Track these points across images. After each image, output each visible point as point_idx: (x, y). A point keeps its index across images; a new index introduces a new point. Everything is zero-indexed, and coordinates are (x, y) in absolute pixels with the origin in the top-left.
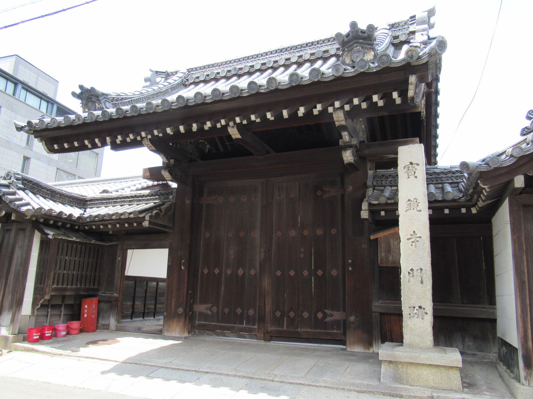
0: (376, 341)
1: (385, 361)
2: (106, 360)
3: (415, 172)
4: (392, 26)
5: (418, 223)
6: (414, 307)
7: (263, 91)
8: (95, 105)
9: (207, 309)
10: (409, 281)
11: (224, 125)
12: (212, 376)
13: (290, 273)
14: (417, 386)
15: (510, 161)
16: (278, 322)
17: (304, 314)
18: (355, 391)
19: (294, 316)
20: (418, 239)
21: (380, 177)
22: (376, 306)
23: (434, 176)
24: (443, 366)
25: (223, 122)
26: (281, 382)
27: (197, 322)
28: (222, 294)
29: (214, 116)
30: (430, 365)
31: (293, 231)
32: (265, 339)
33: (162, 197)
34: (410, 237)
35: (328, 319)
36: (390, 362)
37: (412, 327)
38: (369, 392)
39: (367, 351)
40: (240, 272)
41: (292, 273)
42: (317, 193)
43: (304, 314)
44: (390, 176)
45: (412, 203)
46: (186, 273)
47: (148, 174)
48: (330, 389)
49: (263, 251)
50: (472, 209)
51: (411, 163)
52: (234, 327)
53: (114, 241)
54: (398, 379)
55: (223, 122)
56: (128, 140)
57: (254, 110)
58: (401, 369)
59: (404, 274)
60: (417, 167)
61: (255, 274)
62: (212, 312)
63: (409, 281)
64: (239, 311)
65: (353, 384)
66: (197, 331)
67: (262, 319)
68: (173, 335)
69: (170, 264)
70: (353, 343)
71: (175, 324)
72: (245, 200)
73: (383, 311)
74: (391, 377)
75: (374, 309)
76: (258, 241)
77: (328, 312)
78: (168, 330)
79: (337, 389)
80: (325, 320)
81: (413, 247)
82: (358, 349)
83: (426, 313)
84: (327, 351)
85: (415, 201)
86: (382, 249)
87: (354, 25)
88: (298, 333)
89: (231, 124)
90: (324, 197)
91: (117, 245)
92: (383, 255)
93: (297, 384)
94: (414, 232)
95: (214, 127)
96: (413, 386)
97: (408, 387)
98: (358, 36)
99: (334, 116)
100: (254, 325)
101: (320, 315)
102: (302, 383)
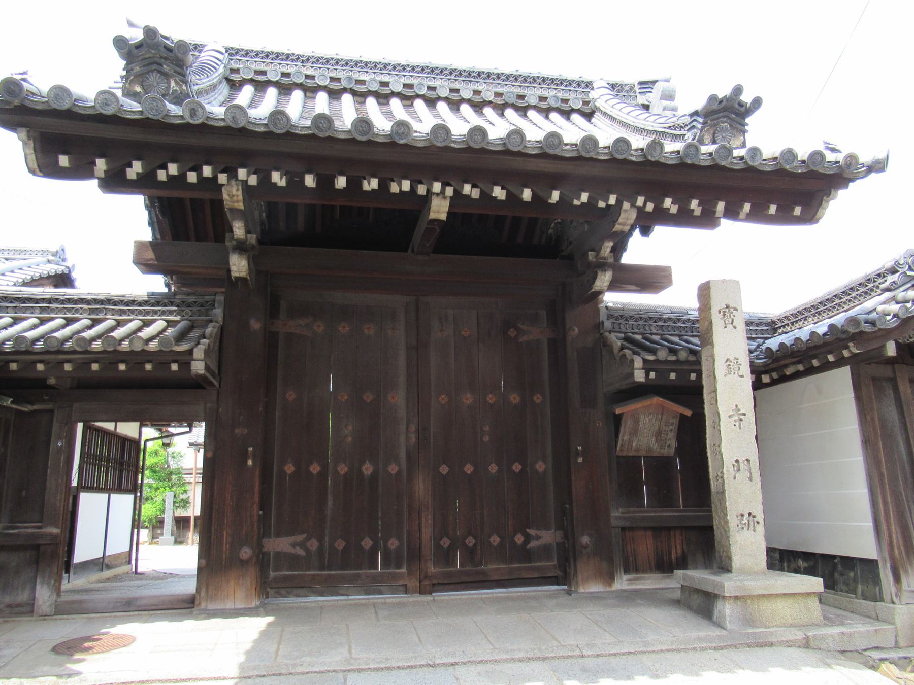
2: (190, 679)
4: (232, 52)
6: (742, 515)
7: (633, 159)
8: (169, 83)
9: (294, 545)
10: (735, 478)
11: (174, 176)
12: (480, 668)
13: (465, 469)
16: (445, 557)
17: (492, 540)
18: (710, 648)
19: (475, 545)
20: (742, 417)
22: (617, 518)
23: (688, 325)
24: (799, 594)
26: (598, 656)
27: (272, 574)
28: (329, 513)
29: (601, 186)
31: (469, 395)
32: (422, 592)
33: (187, 310)
35: (533, 544)
36: (737, 598)
39: (608, 589)
40: (368, 469)
41: (469, 469)
42: (509, 333)
43: (492, 540)
46: (257, 473)
47: (150, 255)
49: (413, 428)
50: (763, 376)
51: (727, 307)
52: (358, 576)
53: (43, 401)
54: (749, 621)
55: (173, 169)
56: (162, 175)
57: (311, 163)
60: (735, 313)
61: (399, 473)
62: (307, 550)
63: (735, 478)
64: (367, 543)
65: (699, 639)
66: (271, 592)
67: (415, 555)
68: (229, 605)
69: (210, 455)
70: (587, 580)
71: (232, 583)
72: (372, 332)
73: (627, 524)
75: (614, 522)
76: (402, 412)
77: (532, 532)
78: (212, 598)
79: (685, 650)
80: (528, 547)
82: (595, 587)
83: (758, 523)
86: (627, 430)
87: (738, 90)
88: (483, 573)
89: (626, 205)
90: (521, 340)
91: (52, 411)
93: (623, 654)
94: (736, 406)
95: (591, 204)
98: (733, 107)
100: (399, 567)
101: (519, 539)
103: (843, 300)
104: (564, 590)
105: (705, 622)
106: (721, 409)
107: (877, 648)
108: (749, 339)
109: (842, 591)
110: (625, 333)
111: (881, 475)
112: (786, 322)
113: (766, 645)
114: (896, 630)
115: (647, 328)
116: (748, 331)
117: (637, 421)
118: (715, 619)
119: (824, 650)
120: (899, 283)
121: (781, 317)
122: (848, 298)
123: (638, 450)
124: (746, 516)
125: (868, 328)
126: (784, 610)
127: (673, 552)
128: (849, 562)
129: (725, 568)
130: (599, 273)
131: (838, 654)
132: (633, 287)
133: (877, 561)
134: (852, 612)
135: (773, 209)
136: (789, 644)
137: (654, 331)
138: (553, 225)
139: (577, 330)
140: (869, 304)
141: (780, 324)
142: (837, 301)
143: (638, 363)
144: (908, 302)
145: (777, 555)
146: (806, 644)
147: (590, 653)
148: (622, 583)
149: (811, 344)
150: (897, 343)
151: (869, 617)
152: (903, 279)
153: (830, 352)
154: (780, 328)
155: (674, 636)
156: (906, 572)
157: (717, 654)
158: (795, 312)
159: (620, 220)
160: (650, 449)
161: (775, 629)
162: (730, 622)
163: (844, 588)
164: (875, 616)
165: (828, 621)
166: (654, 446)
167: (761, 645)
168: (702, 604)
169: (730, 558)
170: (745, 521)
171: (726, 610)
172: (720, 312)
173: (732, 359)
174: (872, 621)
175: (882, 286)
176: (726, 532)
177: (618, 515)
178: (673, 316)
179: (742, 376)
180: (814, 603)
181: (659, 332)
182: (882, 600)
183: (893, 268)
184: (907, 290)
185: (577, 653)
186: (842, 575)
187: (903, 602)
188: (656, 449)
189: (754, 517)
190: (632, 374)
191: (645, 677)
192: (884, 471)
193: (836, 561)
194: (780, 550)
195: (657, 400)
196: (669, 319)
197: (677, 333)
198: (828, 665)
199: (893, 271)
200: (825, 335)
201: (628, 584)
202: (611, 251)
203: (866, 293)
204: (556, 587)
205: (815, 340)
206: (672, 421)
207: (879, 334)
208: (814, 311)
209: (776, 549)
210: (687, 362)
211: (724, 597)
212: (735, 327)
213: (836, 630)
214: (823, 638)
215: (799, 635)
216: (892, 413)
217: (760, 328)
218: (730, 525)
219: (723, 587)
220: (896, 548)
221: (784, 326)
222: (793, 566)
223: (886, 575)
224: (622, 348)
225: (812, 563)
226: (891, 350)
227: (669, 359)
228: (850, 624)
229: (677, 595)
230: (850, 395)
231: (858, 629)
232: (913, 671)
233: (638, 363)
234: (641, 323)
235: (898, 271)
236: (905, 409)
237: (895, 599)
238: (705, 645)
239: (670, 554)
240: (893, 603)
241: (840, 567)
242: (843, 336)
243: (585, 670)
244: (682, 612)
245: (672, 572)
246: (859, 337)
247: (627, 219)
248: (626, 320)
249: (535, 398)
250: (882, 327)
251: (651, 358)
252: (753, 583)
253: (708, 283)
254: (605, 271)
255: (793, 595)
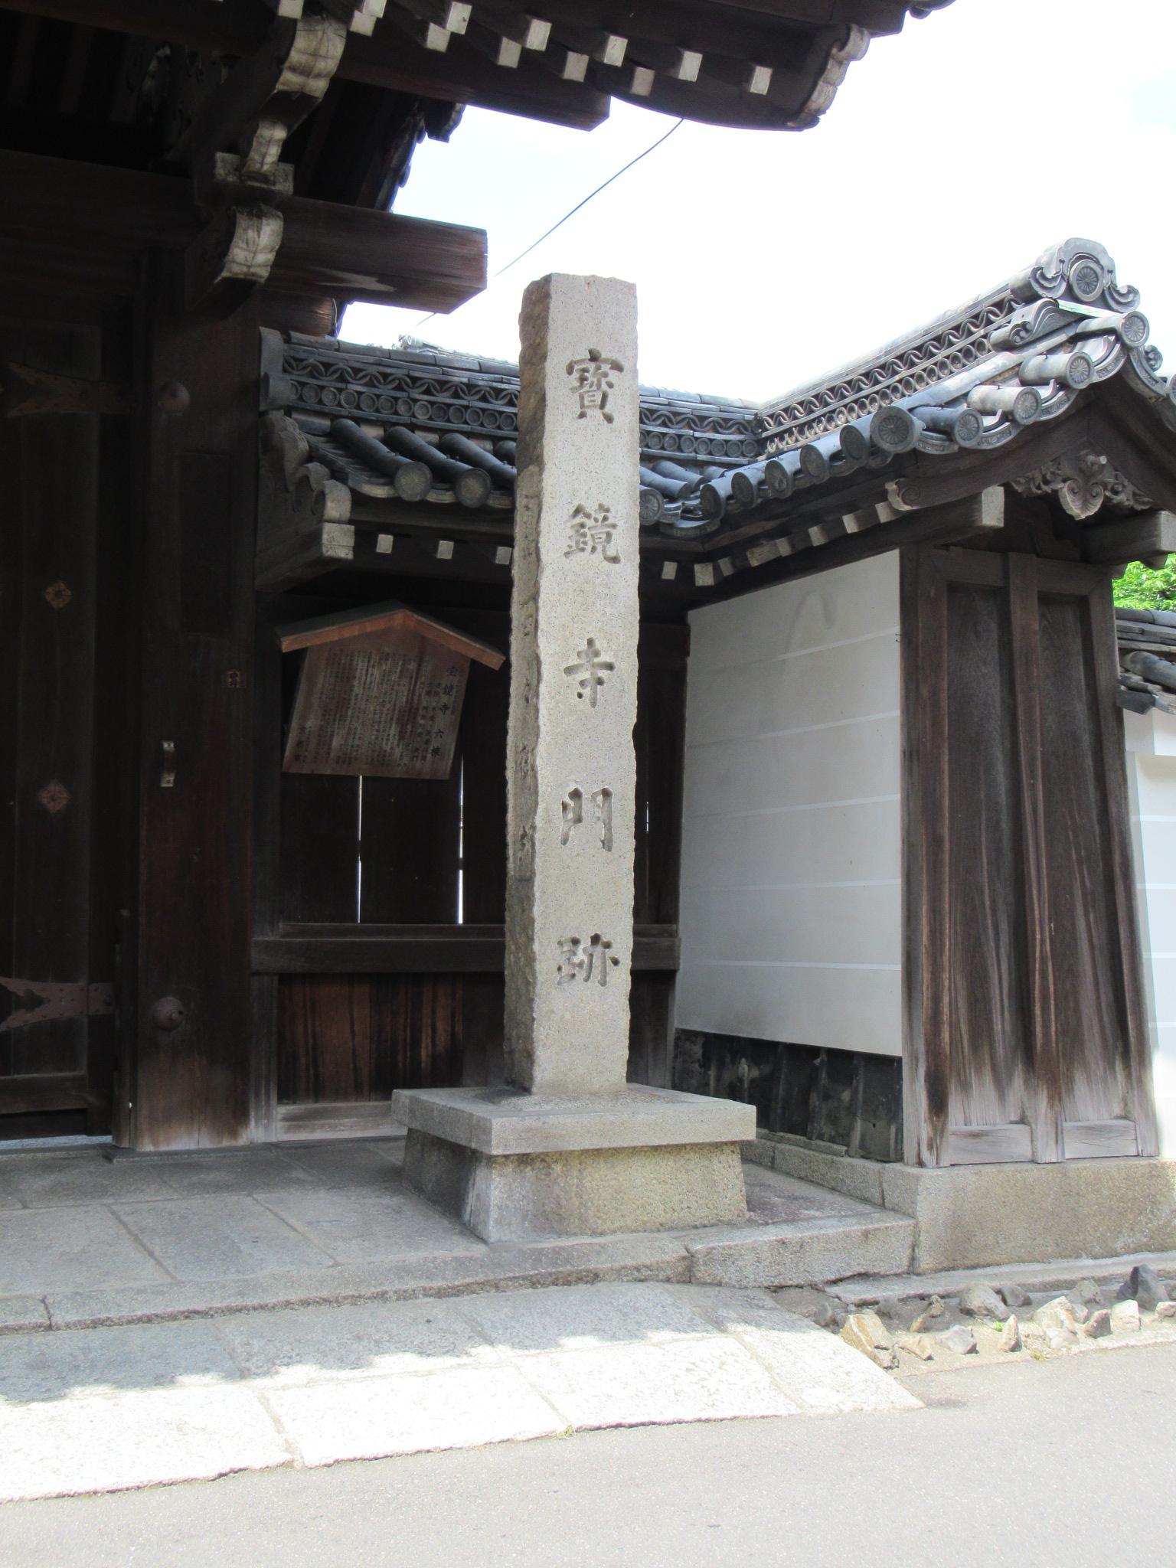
0: (257, 1095)
1: (507, 1157)
3: (605, 397)
5: (608, 610)
6: (575, 942)
10: (565, 841)
14: (614, 1232)
15: (1001, 432)
18: (427, 1293)
20: (603, 674)
21: (314, 372)
22: (267, 947)
25: (539, 34)
26: (96, 1324)
30: (656, 1149)
34: (573, 661)
36: (524, 1159)
37: (568, 1016)
38: (482, 1285)
39: (226, 1143)
44: (357, 371)
45: (590, 523)
48: (325, 1308)
50: (697, 567)
51: (594, 357)
54: (550, 1218)
58: (562, 1182)
59: (546, 809)
60: (613, 376)
63: (565, 841)
65: (403, 1271)
70: (168, 1118)
73: (298, 965)
74: (524, 1218)
75: (258, 959)
79: (355, 1300)
81: (584, 705)
82: (187, 1140)
83: (616, 962)
84: (47, 1167)
85: (600, 517)
92: (312, 723)
93: (173, 1317)
94: (590, 642)
96: (602, 1234)
97: (587, 1240)
99: (301, 42)
102: (201, 1306)
103: (916, 370)
104: (101, 1146)
105: (442, 1224)
106: (546, 648)
107: (863, 1276)
108: (646, 459)
109: (821, 1137)
110: (334, 417)
111: (936, 841)
112: (788, 423)
113: (579, 1280)
114: (916, 1230)
115: (402, 408)
116: (645, 434)
117: (344, 676)
118: (466, 1217)
119: (727, 1285)
120: (1037, 329)
121: (777, 410)
122: (928, 364)
123: (346, 759)
124: (586, 943)
125: (934, 446)
126: (649, 1187)
127: (426, 1041)
128: (843, 1062)
129: (519, 1084)
130: (242, 222)
131: (768, 1301)
132: (371, 283)
133: (899, 1060)
134: (833, 1189)
135: (690, 66)
136: (641, 1275)
137: (422, 418)
138: (153, 66)
139: (184, 395)
140: (953, 383)
141: (773, 429)
142: (904, 373)
143: (337, 504)
144: (1043, 382)
145: (697, 1050)
146: (687, 1273)
147: (72, 1317)
148: (270, 1126)
149: (804, 483)
150: (1010, 493)
151: (865, 1200)
152: (1050, 321)
153: (851, 508)
154: (771, 439)
155: (337, 1264)
156: (965, 1087)
157: (438, 1309)
158: (808, 397)
159: (295, 56)
160: (381, 759)
161: (619, 1236)
162: (498, 1222)
163: (827, 1130)
164: (877, 1196)
165: (758, 1208)
166: (392, 743)
167: (566, 1281)
168: (440, 1178)
169: (529, 1056)
170: (581, 956)
171: (495, 1192)
172: (570, 370)
173: (590, 507)
174: (868, 1208)
175: (997, 335)
176: (529, 984)
177: (271, 940)
178: (482, 380)
179: (615, 560)
180: (730, 1172)
181: (440, 424)
182: (900, 1158)
183: (1028, 285)
184: (1051, 351)
185: (38, 1317)
186: (811, 1101)
187: (946, 1160)
188: (401, 760)
189: (608, 945)
190: (315, 537)
191: (207, 1378)
192: (946, 832)
193: (817, 1062)
194: (706, 1035)
195: (401, 619)
196: (470, 387)
197: (490, 429)
198: (719, 1325)
199: (1026, 294)
200: (835, 456)
201: (288, 1130)
202: (283, 158)
203: (967, 354)
204: (81, 1140)
205: (812, 468)
206: (446, 681)
207: (964, 464)
208: (851, 397)
209: (696, 1034)
210: (482, 512)
211: (491, 1160)
212: (609, 419)
213: (770, 1234)
214: (729, 1257)
215: (669, 1250)
216: (988, 685)
217: (670, 431)
218: (538, 966)
219: (487, 1131)
220: (946, 1028)
221: (780, 436)
222: (727, 1077)
223: (913, 1092)
224: (312, 456)
225: (767, 1069)
226: (992, 509)
227: (433, 497)
228: (808, 1219)
229: (396, 1156)
230: (892, 628)
231: (827, 1232)
232: (1174, 1316)
233: (337, 504)
234: (386, 391)
235: (1036, 297)
236: (1019, 672)
237: (926, 1155)
238: (412, 1284)
239: (416, 1043)
240: (921, 1164)
241: (824, 1079)
242: (874, 463)
243: (40, 1364)
244: (395, 1201)
245: (387, 1096)
246: (910, 466)
247: (315, 54)
248: (342, 379)
249: (49, 594)
250: (968, 444)
251: (378, 491)
252: (569, 1120)
253: (547, 279)
254: (260, 216)
255: (678, 1149)
